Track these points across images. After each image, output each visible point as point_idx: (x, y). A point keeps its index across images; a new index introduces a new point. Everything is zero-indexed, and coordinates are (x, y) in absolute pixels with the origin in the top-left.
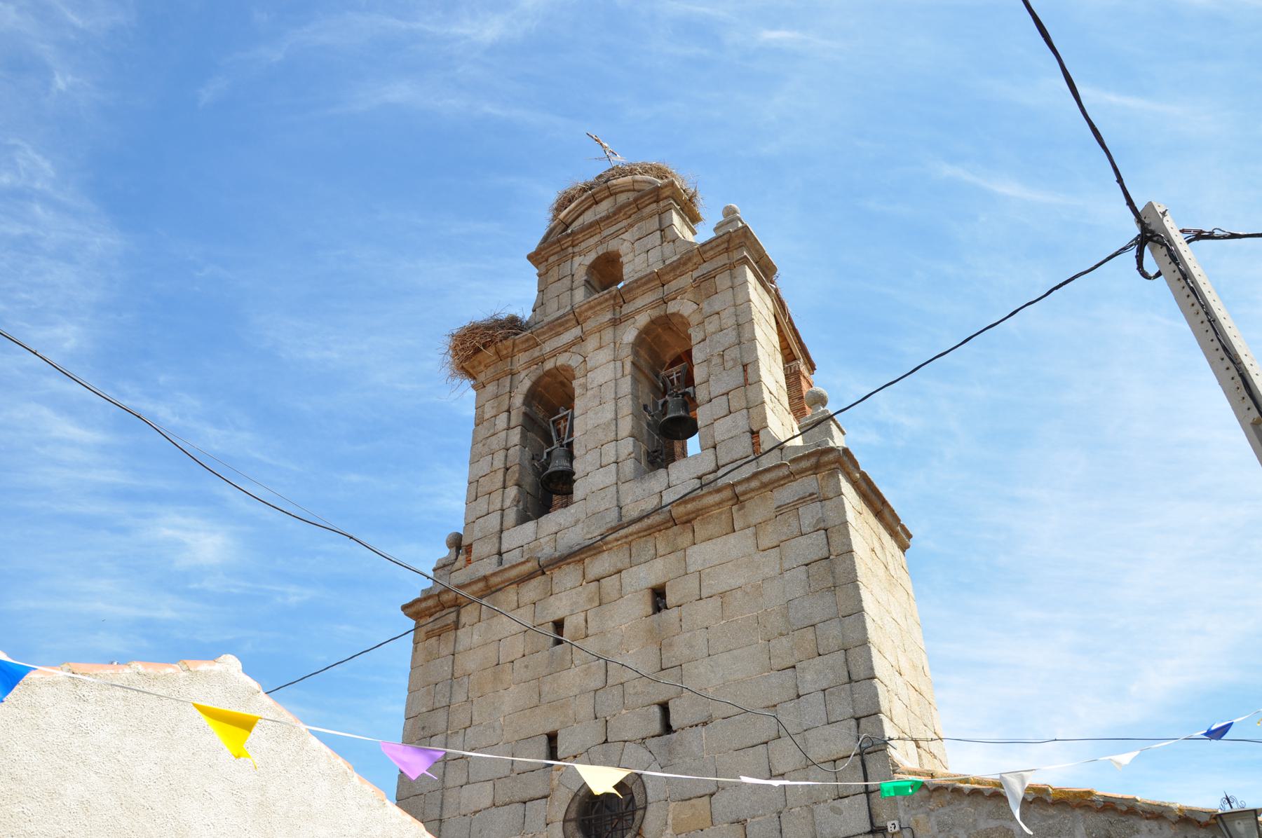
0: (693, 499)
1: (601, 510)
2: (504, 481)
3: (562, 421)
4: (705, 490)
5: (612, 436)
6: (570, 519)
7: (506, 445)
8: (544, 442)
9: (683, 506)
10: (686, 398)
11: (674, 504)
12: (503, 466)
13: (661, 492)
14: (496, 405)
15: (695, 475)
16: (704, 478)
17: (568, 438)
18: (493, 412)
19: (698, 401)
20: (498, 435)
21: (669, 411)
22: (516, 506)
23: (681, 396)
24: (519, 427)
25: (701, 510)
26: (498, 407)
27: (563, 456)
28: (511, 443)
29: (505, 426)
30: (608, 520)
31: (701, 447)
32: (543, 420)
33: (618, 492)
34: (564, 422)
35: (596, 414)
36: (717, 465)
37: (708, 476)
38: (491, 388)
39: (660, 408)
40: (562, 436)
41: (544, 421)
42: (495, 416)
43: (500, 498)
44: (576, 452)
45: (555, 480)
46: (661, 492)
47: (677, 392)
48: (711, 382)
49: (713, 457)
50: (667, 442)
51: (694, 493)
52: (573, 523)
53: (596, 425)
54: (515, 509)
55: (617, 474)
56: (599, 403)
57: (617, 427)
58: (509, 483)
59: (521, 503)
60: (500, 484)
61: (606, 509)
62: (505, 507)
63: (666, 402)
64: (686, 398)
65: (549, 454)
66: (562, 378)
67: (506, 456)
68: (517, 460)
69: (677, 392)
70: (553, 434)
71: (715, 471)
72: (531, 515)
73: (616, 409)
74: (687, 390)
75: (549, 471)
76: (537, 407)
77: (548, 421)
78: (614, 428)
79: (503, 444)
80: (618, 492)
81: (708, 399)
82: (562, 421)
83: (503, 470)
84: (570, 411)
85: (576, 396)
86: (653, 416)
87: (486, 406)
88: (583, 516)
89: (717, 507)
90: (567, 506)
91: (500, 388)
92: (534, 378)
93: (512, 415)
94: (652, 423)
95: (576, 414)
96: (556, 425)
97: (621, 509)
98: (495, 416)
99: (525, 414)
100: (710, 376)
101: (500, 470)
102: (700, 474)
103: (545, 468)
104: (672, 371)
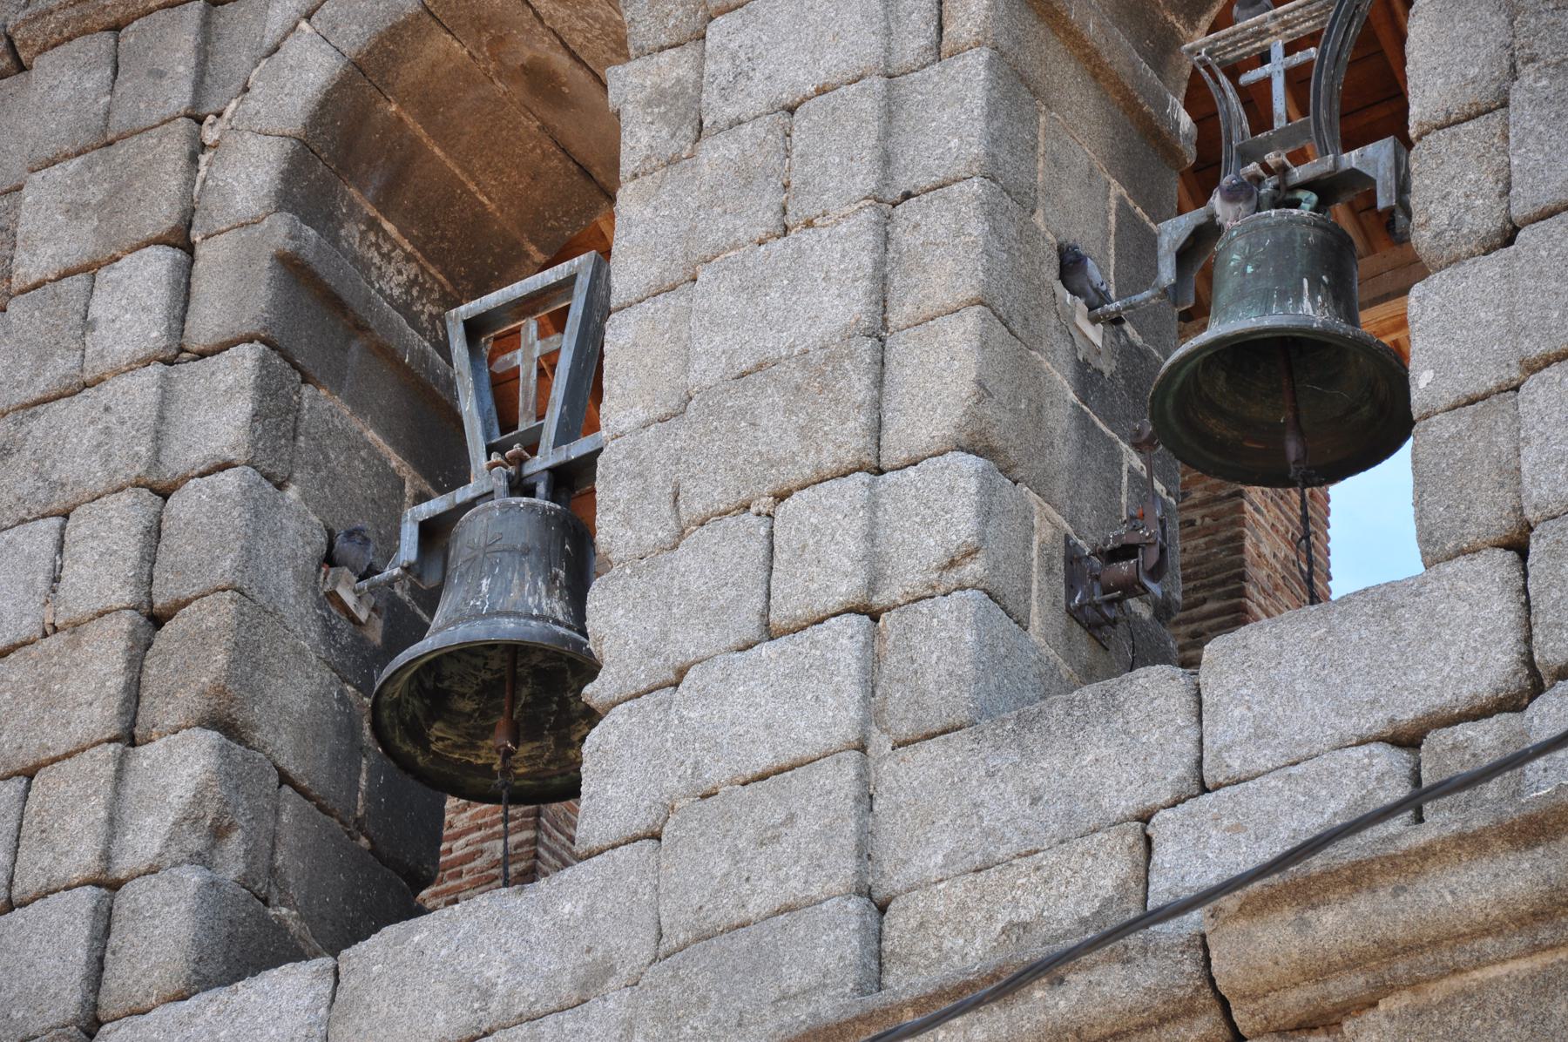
0: (1358, 877)
1: (752, 911)
2: (133, 695)
3: (530, 327)
4: (1441, 821)
5: (849, 438)
6: (545, 961)
7: (156, 460)
8: (412, 456)
9: (1289, 914)
10: (1340, 213)
11: (1230, 902)
12: (126, 596)
13: (1145, 818)
14: (95, 194)
15: (1376, 721)
16: (1437, 740)
17: (566, 435)
18: (77, 243)
19: (1422, 240)
20: (105, 394)
21: (1223, 296)
22: (201, 859)
23: (1309, 198)
24: (248, 356)
25: (1411, 948)
26: (110, 207)
27: (526, 552)
28: (185, 453)
29: (154, 335)
30: (795, 978)
31: (1426, 538)
32: (405, 308)
33: (867, 799)
34: (542, 334)
35: (753, 289)
36: (1529, 661)
37: (1465, 731)
38: (69, 76)
39: (1167, 273)
40: (523, 426)
41: (413, 320)
42: (90, 269)
43: (97, 808)
44: (608, 530)
45: (467, 706)
46: (1145, 818)
47: (1283, 170)
48: (1523, 113)
49: (1501, 609)
50: (1197, 495)
51: (1358, 840)
52: (567, 991)
53: (746, 363)
54: (193, 877)
55: (870, 687)
56: (770, 218)
57: (879, 383)
58: (160, 710)
59: (235, 844)
60: (101, 716)
61: (789, 909)
62: (122, 867)
63: (1206, 234)
64: (1340, 213)
65: (434, 533)
66: (543, 49)
67: (155, 533)
68: (227, 563)
69: (1283, 170)
70: (468, 406)
71: (1511, 703)
72: (294, 926)
73: (879, 265)
74: (1352, 159)
75: (428, 644)
76: (373, 224)
77: (441, 318)
78: (859, 387)
79: (132, 455)
80: (867, 799)
81: (1490, 224)
82: (530, 327)
83: (125, 622)
84: (582, 263)
85: (628, 164)
86: (1117, 321)
87: (28, 196)
88: (634, 948)
89: (1518, 942)
90: (530, 875)
91: (125, 86)
92: (355, 37)
93: (199, 265)
94: (1107, 366)
95: (626, 276)
96: (487, 343)
97: (882, 909)
98: (90, 269)
99: (291, 267)
100: (1514, 73)
101: (108, 623)
102: (1408, 713)
103: (406, 627)
104: (1261, 34)
